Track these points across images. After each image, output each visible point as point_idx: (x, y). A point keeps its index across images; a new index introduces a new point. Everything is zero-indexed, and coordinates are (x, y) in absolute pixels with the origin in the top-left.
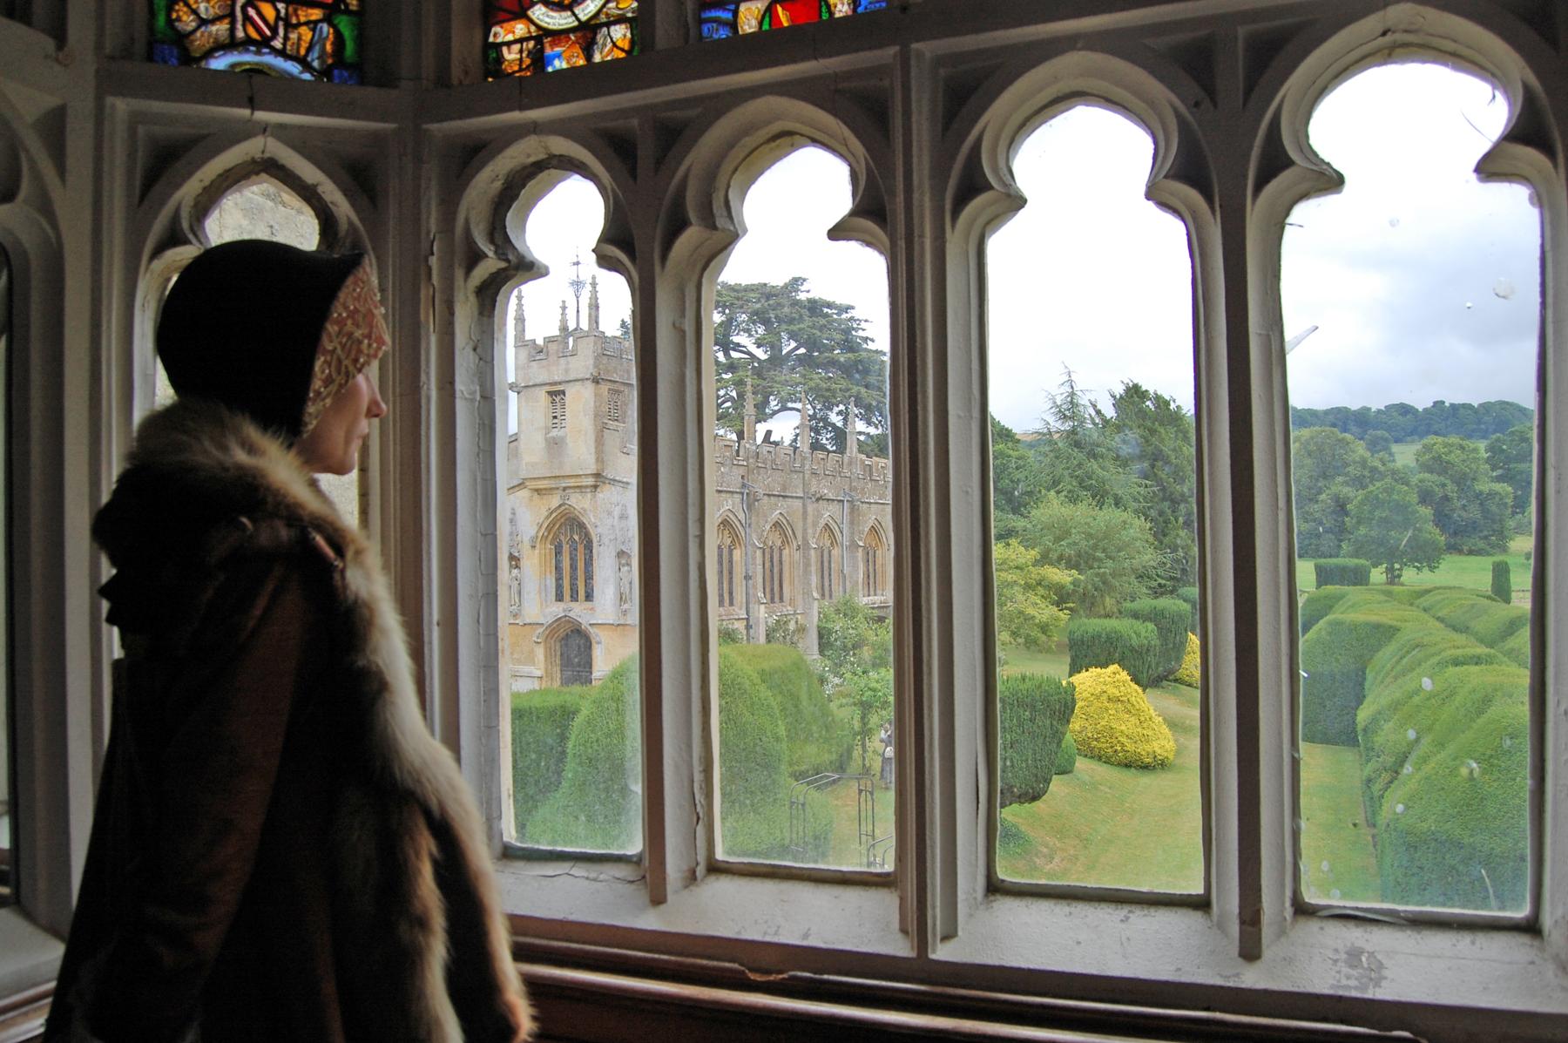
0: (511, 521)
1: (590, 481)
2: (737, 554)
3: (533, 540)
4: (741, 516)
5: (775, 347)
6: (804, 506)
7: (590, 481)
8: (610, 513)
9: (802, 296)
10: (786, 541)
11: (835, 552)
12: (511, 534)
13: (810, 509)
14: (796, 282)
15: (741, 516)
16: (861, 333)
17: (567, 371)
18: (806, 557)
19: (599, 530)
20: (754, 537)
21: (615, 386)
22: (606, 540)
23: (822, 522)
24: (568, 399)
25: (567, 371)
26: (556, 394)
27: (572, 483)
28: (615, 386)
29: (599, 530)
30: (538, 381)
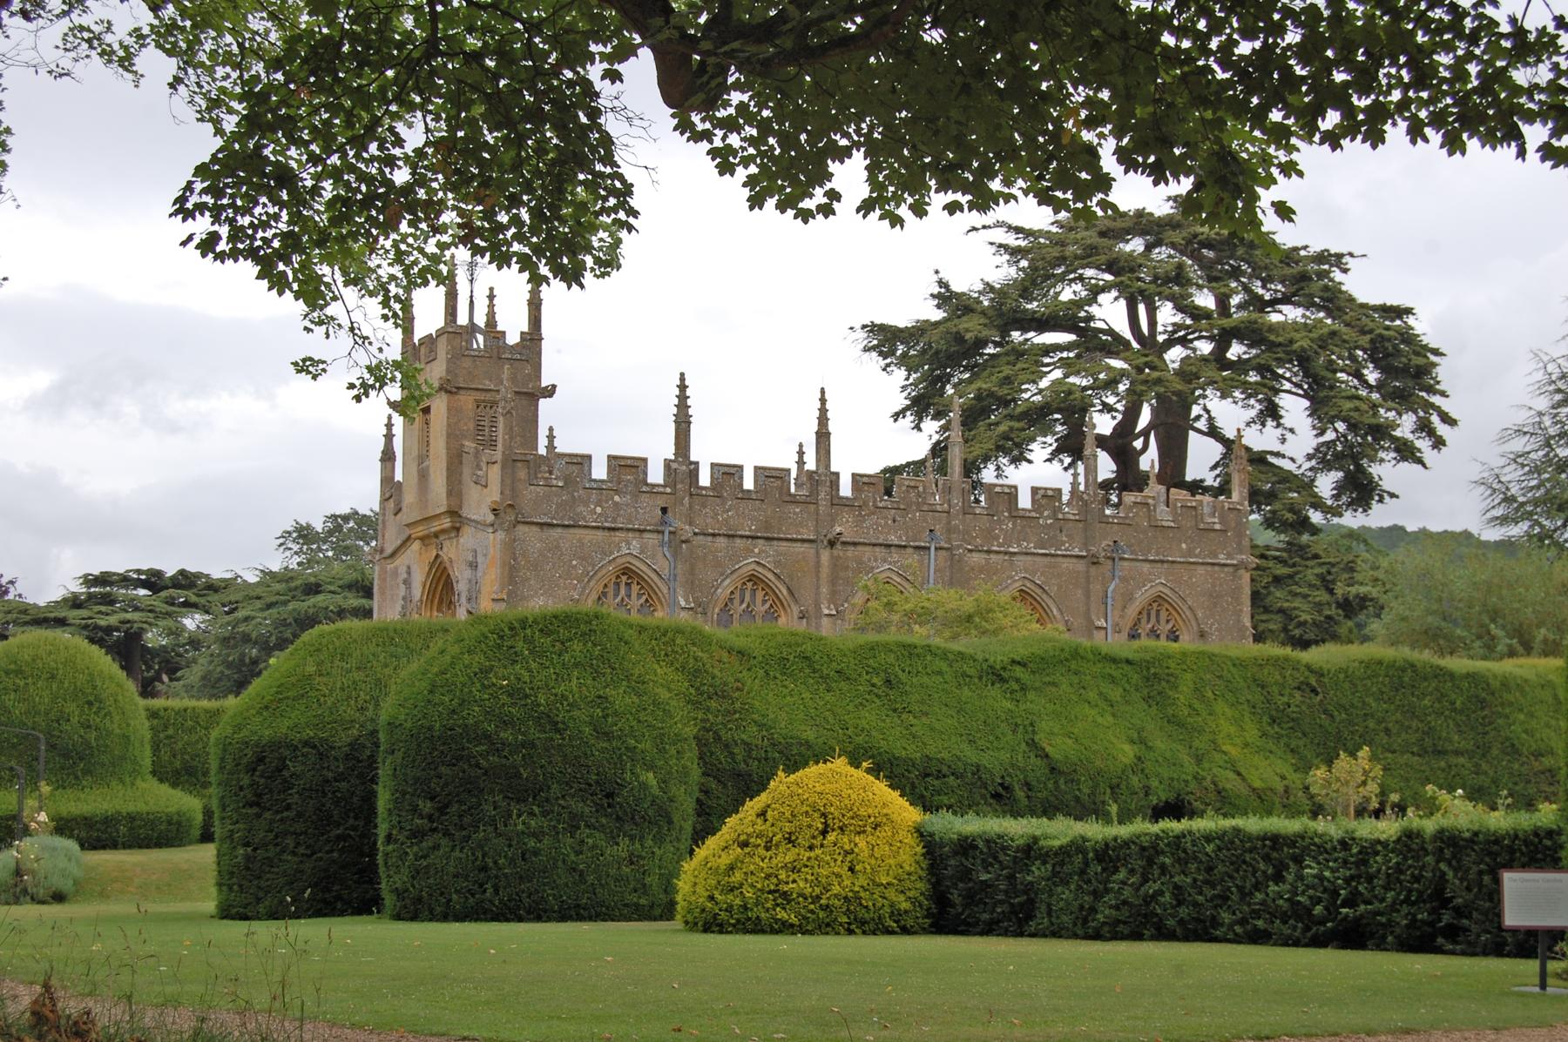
1: (446, 523)
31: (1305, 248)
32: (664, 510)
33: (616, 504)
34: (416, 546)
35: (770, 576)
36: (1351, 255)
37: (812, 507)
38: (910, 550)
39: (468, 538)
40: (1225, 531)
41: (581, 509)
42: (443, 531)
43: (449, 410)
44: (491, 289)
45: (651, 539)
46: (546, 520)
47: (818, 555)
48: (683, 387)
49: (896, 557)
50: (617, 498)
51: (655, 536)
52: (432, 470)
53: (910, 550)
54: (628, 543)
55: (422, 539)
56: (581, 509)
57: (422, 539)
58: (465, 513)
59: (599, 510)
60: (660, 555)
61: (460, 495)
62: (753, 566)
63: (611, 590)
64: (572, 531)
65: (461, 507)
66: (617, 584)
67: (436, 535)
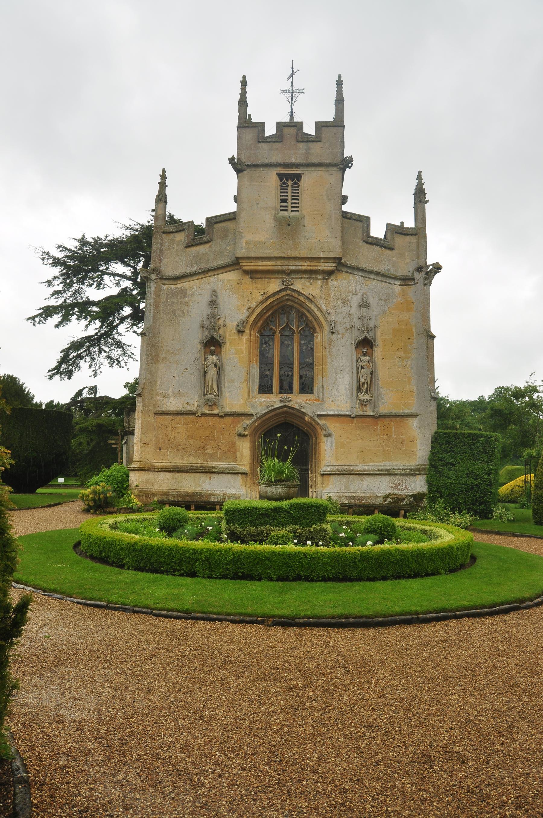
7: (329, 266)
19: (332, 318)
48: (163, 177)
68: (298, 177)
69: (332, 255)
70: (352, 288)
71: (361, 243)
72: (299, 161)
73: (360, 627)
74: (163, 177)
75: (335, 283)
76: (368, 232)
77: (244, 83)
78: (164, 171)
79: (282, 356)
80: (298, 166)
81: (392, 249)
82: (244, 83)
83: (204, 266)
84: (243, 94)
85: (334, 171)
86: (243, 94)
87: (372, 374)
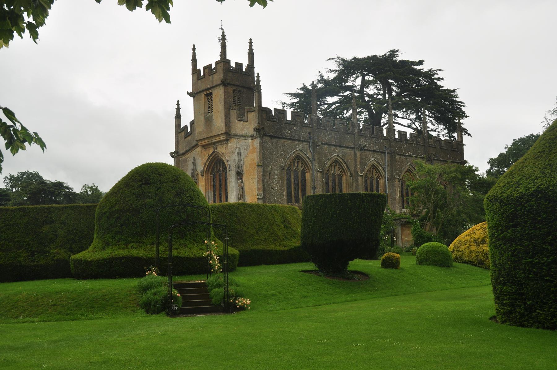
0: (193, 163)
1: (223, 137)
2: (308, 175)
3: (202, 172)
4: (309, 155)
5: (424, 110)
6: (355, 154)
7: (223, 137)
8: (233, 153)
9: (398, 59)
10: (343, 171)
11: (381, 181)
12: (193, 170)
13: (358, 154)
14: (393, 53)
15: (309, 155)
16: (436, 76)
17: (212, 82)
18: (357, 181)
19: (229, 163)
20: (317, 165)
21: (238, 88)
22: (232, 168)
23: (369, 164)
24: (213, 96)
25: (212, 82)
26: (209, 96)
27: (216, 139)
28: (238, 88)
29: (229, 163)
30: (201, 89)
31: (421, 62)
32: (309, 134)
33: (295, 130)
34: (198, 149)
35: (341, 161)
36: (439, 70)
37: (353, 135)
38: (379, 153)
39: (234, 144)
40: (458, 151)
41: (284, 131)
42: (220, 141)
43: (225, 92)
44: (194, 46)
45: (306, 145)
46: (273, 134)
47: (355, 154)
48: (178, 105)
49: (376, 156)
50: (295, 128)
51: (306, 143)
52: (214, 118)
53: (379, 153)
54: (299, 146)
55: (203, 146)
56: (284, 131)
57: (203, 146)
58: (233, 132)
59: (289, 132)
60: (309, 151)
61: (230, 126)
62: (336, 157)
63: (292, 164)
64: (281, 140)
65: (230, 131)
66: (294, 162)
67: (214, 143)
68: (211, 94)
69: (222, 132)
70: (235, 146)
71: (237, 122)
72: (211, 86)
73: (198, 258)
74: (178, 105)
75: (230, 145)
76: (261, 105)
77: (194, 49)
78: (178, 101)
79: (295, 194)
80: (210, 89)
81: (247, 121)
82: (194, 49)
83: (191, 146)
84: (194, 54)
85: (228, 81)
86: (194, 54)
87: (242, 189)
